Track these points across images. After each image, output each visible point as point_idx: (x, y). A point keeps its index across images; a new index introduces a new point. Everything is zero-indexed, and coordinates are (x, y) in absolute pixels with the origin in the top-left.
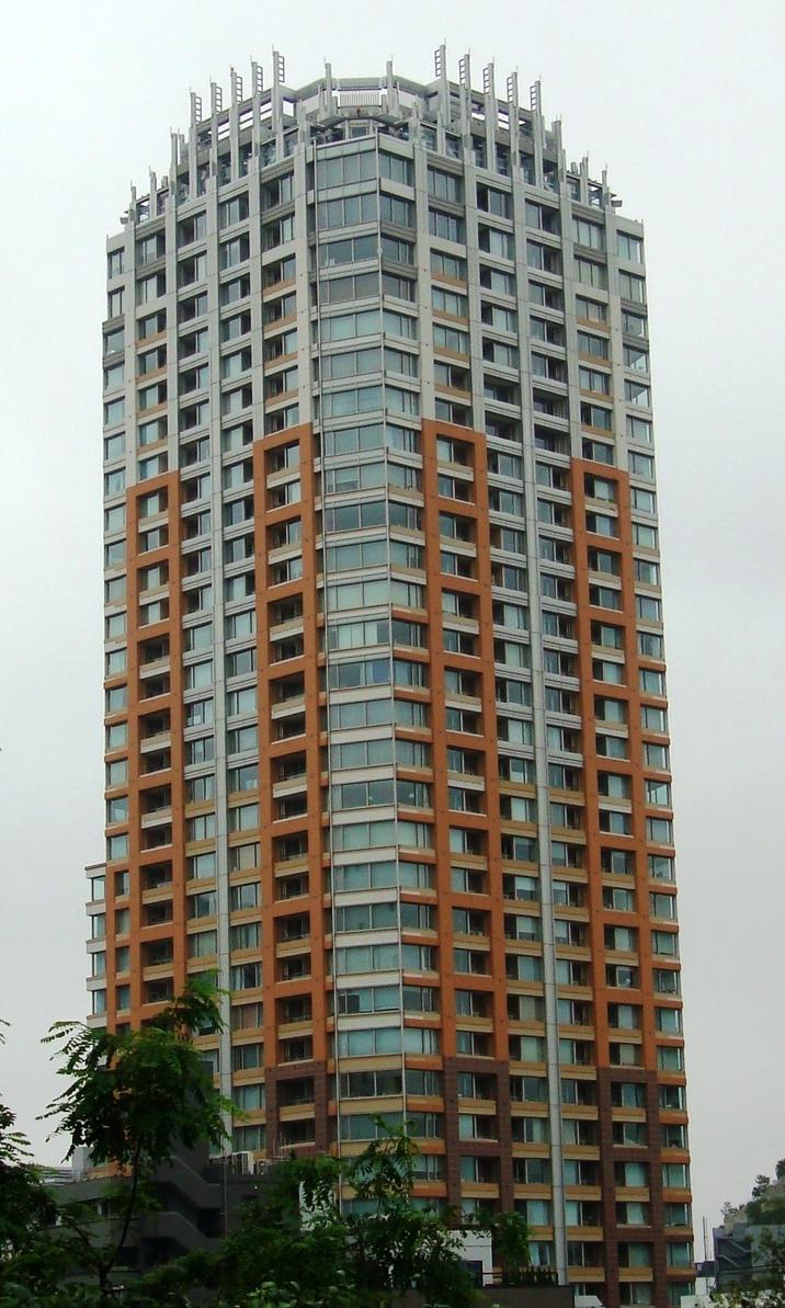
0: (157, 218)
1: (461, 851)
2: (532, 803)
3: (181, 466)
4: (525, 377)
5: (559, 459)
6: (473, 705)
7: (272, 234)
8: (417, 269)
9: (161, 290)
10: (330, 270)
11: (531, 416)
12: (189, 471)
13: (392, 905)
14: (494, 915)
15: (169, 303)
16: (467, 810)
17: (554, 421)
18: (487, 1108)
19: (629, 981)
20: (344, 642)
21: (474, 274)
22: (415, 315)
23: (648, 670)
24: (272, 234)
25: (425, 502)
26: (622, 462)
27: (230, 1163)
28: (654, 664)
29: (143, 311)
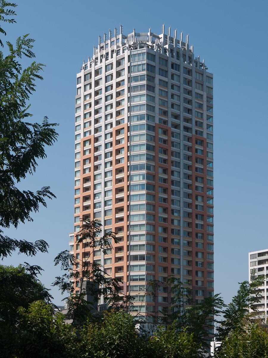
0: (90, 69)
1: (161, 232)
2: (179, 221)
3: (95, 133)
4: (181, 113)
5: (189, 134)
6: (165, 196)
7: (119, 74)
8: (155, 84)
9: (91, 88)
10: (134, 84)
11: (183, 124)
12: (97, 135)
13: (144, 245)
14: (169, 248)
15: (92, 91)
16: (163, 222)
17: (188, 125)
18: (166, 295)
19: (201, 265)
20: (134, 180)
21: (170, 96)
22: (154, 116)
23: (209, 226)
24: (119, 74)
25: (155, 164)
26: (205, 136)
27: (103, 306)
28: (211, 215)
29: (86, 93)
